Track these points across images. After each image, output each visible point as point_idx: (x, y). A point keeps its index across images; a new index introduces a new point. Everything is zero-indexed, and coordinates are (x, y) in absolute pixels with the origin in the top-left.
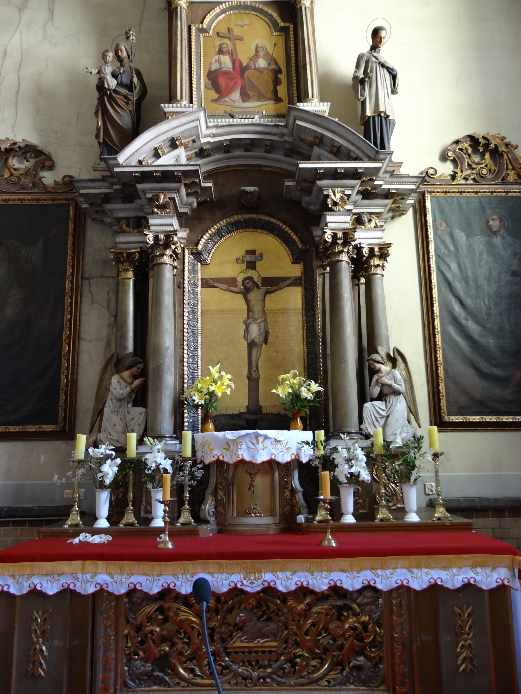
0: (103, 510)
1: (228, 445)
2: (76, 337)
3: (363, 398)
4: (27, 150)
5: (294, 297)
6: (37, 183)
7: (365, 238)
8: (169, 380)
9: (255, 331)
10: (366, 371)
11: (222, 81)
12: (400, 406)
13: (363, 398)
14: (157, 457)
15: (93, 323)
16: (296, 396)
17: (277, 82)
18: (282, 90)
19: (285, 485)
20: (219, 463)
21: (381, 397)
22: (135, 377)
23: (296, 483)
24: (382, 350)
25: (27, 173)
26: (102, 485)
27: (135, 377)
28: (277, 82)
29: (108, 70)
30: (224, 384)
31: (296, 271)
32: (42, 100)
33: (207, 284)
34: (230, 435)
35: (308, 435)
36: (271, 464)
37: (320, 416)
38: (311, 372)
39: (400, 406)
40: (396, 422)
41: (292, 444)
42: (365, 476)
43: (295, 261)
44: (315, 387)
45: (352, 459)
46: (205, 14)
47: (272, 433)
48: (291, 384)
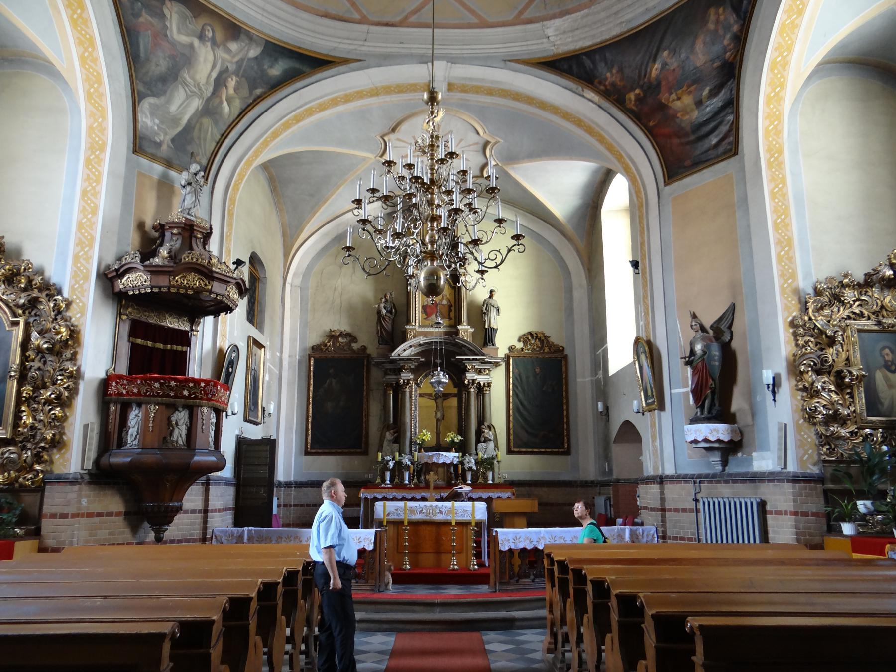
0: (388, 478)
1: (429, 457)
2: (368, 415)
3: (478, 441)
4: (348, 335)
5: (454, 402)
6: (351, 349)
7: (482, 379)
8: (408, 434)
9: (439, 415)
10: (479, 432)
11: (428, 310)
12: (491, 445)
13: (478, 441)
14: (406, 461)
15: (375, 409)
16: (453, 440)
17: (450, 311)
18: (452, 314)
19: (448, 471)
20: (426, 464)
21: (485, 441)
22: (395, 432)
23: (452, 470)
24: (486, 424)
25: (347, 344)
26: (388, 470)
27: (395, 432)
28: (450, 311)
29: (382, 305)
30: (427, 436)
31: (455, 391)
32: (351, 311)
33: (421, 395)
34: (430, 454)
35: (457, 455)
36: (444, 464)
37: (462, 448)
38: (460, 432)
39: (491, 445)
40: (486, 451)
41: (451, 457)
42: (474, 468)
43: (455, 387)
44: (460, 438)
45: (471, 462)
46: (399, 117)
47: (444, 454)
48: (452, 436)
